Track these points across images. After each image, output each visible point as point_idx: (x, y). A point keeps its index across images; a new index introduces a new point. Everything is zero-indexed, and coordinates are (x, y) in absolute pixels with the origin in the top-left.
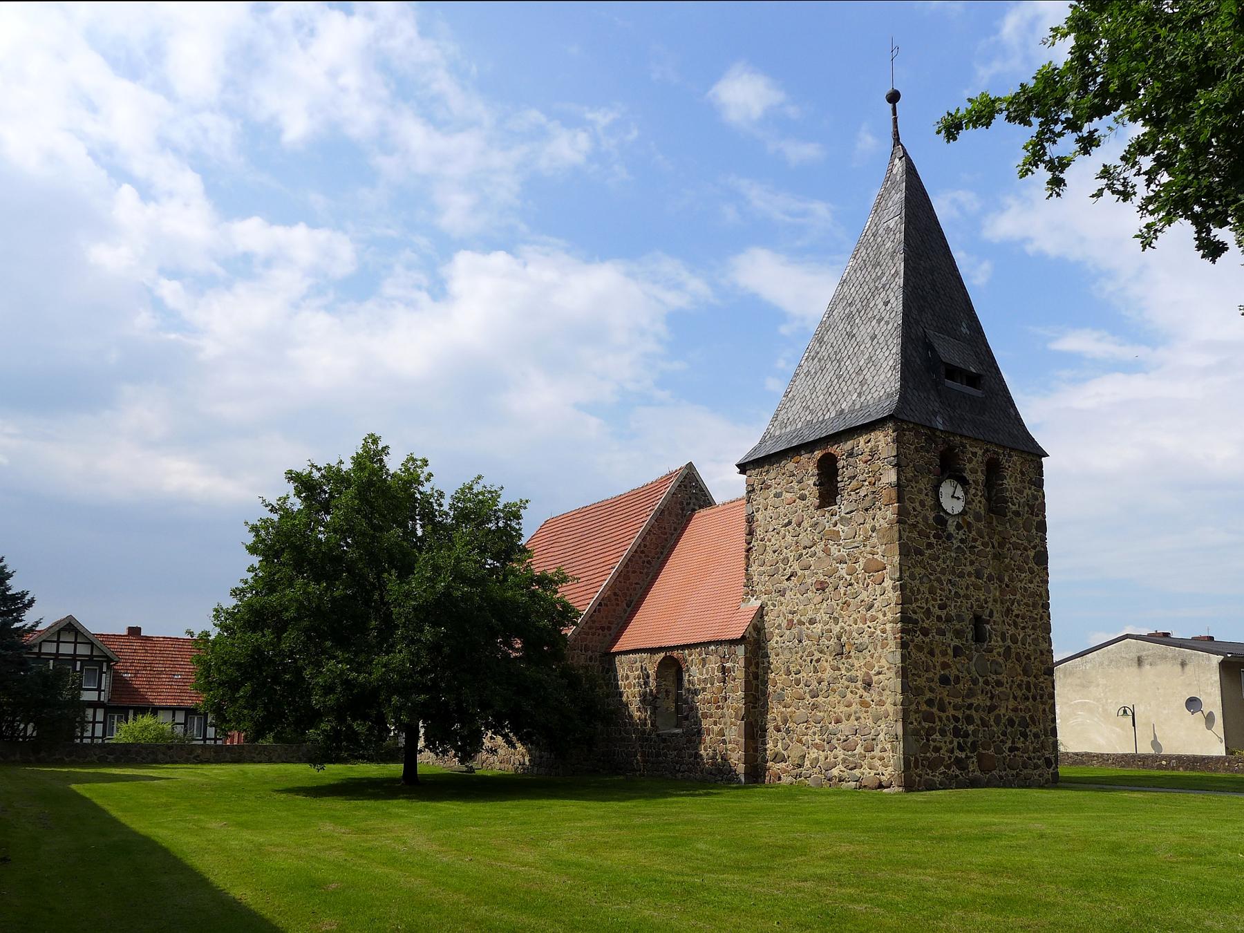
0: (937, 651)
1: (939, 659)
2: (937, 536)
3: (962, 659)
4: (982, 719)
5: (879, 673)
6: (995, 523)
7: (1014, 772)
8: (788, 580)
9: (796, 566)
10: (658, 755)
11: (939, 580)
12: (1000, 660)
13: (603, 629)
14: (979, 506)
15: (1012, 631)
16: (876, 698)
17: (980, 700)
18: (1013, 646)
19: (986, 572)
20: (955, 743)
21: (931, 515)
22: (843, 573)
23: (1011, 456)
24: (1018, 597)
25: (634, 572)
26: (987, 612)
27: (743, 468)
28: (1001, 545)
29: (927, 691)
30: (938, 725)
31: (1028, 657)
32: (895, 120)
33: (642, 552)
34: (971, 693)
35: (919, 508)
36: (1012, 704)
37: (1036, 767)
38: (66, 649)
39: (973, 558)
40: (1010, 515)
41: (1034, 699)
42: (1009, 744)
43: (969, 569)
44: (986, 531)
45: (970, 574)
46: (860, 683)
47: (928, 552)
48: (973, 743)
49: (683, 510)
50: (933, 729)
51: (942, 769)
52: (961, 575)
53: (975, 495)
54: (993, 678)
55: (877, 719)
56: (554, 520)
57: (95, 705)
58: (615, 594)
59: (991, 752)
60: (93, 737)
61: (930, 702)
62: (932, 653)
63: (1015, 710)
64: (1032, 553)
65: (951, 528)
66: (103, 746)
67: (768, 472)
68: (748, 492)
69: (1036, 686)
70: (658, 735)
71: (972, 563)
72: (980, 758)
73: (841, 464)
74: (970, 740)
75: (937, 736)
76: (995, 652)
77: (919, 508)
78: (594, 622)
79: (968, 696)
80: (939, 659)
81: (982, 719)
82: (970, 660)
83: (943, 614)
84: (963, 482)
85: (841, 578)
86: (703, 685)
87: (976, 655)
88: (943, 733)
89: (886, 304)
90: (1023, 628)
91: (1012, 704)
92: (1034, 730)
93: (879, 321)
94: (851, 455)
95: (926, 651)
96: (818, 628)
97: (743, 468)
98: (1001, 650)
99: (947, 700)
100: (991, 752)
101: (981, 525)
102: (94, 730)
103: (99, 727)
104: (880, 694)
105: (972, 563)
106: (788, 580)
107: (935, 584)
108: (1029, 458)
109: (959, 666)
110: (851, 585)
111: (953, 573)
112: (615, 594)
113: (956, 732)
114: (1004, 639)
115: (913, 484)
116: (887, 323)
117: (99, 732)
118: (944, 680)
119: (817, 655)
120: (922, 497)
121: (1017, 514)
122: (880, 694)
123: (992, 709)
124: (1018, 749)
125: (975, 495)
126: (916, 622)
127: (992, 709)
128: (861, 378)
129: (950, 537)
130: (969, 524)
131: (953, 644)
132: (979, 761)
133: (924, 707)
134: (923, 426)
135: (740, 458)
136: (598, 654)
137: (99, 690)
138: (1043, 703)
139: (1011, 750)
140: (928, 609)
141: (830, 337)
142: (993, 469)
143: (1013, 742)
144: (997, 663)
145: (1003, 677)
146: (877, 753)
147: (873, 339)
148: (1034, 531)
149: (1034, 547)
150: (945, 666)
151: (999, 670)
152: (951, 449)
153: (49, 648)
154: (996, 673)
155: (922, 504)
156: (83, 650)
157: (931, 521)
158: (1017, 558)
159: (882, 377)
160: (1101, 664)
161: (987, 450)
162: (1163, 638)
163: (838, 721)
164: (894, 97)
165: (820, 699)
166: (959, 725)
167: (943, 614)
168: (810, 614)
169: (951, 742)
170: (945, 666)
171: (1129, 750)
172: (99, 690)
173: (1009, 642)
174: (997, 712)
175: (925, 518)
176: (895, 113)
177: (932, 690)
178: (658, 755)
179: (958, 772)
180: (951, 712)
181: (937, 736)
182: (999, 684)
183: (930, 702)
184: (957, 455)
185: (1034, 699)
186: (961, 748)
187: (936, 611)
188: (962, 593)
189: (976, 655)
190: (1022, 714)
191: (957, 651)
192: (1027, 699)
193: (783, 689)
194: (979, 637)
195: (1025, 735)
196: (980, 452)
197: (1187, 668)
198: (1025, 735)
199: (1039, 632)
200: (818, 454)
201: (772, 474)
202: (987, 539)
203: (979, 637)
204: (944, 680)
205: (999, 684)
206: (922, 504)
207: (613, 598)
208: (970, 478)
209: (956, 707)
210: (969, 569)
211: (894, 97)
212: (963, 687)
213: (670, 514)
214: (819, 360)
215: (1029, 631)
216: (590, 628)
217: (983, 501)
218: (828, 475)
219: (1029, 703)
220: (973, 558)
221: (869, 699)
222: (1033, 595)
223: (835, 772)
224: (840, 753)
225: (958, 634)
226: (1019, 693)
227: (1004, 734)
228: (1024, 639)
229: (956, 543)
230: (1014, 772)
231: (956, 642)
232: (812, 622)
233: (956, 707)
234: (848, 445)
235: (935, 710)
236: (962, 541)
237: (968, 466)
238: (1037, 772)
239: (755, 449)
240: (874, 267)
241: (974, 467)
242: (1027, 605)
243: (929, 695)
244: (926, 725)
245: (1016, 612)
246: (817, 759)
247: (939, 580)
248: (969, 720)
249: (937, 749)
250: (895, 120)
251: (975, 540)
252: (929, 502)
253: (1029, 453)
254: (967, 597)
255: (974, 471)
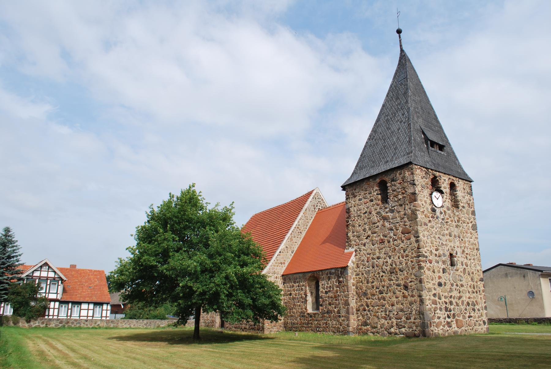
0: (436, 271)
1: (437, 275)
2: (432, 217)
3: (446, 274)
4: (456, 303)
5: (411, 282)
6: (455, 211)
7: (471, 328)
8: (366, 238)
9: (369, 233)
10: (308, 323)
11: (434, 237)
12: (462, 274)
13: (281, 263)
14: (448, 204)
15: (465, 261)
16: (410, 293)
17: (455, 294)
18: (466, 268)
19: (453, 234)
20: (446, 315)
21: (430, 207)
22: (392, 235)
23: (459, 181)
24: (467, 245)
25: (295, 237)
26: (455, 252)
27: (344, 188)
28: (458, 221)
29: (433, 289)
30: (438, 306)
31: (473, 273)
32: (400, 41)
33: (298, 228)
34: (451, 290)
35: (424, 204)
36: (468, 295)
37: (480, 325)
38: (44, 274)
39: (448, 227)
40: (461, 208)
41: (477, 292)
42: (468, 315)
43: (446, 232)
44: (452, 215)
45: (447, 234)
46: (402, 287)
47: (429, 224)
48: (454, 314)
49: (315, 209)
50: (436, 308)
51: (441, 327)
52: (443, 235)
53: (446, 199)
54: (459, 283)
55: (411, 303)
56: (256, 215)
57: (55, 300)
58: (287, 247)
59: (461, 318)
60: (53, 316)
61: (434, 295)
62: (434, 272)
63: (469, 298)
64: (470, 225)
65: (438, 213)
66: (58, 320)
67: (355, 190)
68: (347, 199)
69: (477, 286)
70: (308, 314)
71: (447, 229)
72: (457, 321)
73: (389, 185)
74: (452, 312)
75: (438, 311)
76: (459, 271)
77: (424, 204)
78: (277, 260)
79: (450, 292)
80: (437, 275)
81: (456, 303)
82: (450, 274)
83: (437, 253)
84: (441, 192)
85: (391, 237)
86: (329, 289)
87: (452, 272)
88: (441, 309)
89: (403, 115)
90: (470, 259)
91: (468, 295)
92: (478, 307)
93: (401, 122)
94: (393, 180)
95: (431, 270)
96: (381, 261)
97: (344, 188)
98: (462, 270)
99: (441, 294)
100: (461, 318)
101: (449, 212)
102: (55, 311)
103: (56, 311)
104: (412, 291)
105: (447, 229)
106: (366, 238)
107: (433, 239)
108: (466, 182)
109: (445, 277)
110: (396, 240)
111: (440, 234)
112: (287, 247)
113: (446, 309)
114: (462, 265)
115: (421, 193)
116: (404, 123)
117: (56, 314)
118: (440, 284)
119: (382, 274)
120: (425, 199)
121: (463, 207)
122: (412, 291)
123: (460, 298)
124: (471, 317)
125: (446, 199)
126: (427, 257)
127: (460, 298)
128: (395, 147)
129: (437, 218)
130: (445, 212)
131: (442, 267)
132: (457, 323)
133: (432, 298)
134: (424, 167)
135: (342, 183)
136: (279, 275)
137: (57, 293)
138: (480, 294)
139: (469, 317)
140: (431, 251)
141: (380, 130)
142: (452, 186)
143: (470, 313)
144: (461, 276)
145: (464, 283)
146: (412, 320)
147: (398, 130)
148: (470, 215)
149: (471, 222)
150: (440, 277)
151: (462, 279)
152: (435, 177)
153: (37, 274)
154: (461, 281)
155: (426, 203)
156: (51, 275)
157: (430, 210)
158: (465, 227)
159: (404, 145)
160: (490, 277)
161: (450, 179)
162: (511, 266)
163: (393, 305)
164: (399, 32)
165: (384, 295)
166: (447, 306)
167: (437, 253)
168: (378, 254)
169: (444, 314)
170: (440, 277)
171: (505, 317)
172: (57, 293)
173: (464, 266)
174: (462, 299)
175: (427, 209)
176: (400, 38)
177: (435, 289)
178: (308, 323)
179: (448, 329)
180: (443, 299)
181: (438, 311)
182: (462, 286)
183: (434, 295)
184: (438, 180)
185: (477, 292)
186: (449, 317)
187: (434, 252)
188: (444, 243)
189: (452, 272)
190: (472, 300)
191: (444, 271)
192: (474, 292)
193: (366, 291)
194: (452, 264)
195: (474, 310)
196: (447, 180)
197: (526, 278)
198: (474, 310)
199: (476, 261)
200: (378, 180)
201: (357, 191)
202: (452, 219)
203: (452, 264)
204: (440, 284)
205: (462, 286)
206: (426, 203)
207: (286, 249)
208: (444, 191)
209: (445, 297)
210: (446, 232)
211: (399, 32)
212: (448, 287)
213: (309, 210)
214: (375, 140)
215: (472, 261)
216: (276, 263)
217: (450, 201)
218: (383, 188)
219: (475, 295)
220: (448, 227)
221: (407, 294)
222: (472, 244)
223: (392, 330)
224: (394, 321)
225: (444, 262)
226: (470, 290)
227: (466, 310)
228: (471, 264)
229: (441, 221)
230: (471, 328)
231: (443, 266)
232: (378, 258)
233: (445, 297)
234: (392, 176)
235: (437, 299)
236: (443, 219)
237: (443, 186)
238: (480, 327)
239: (349, 180)
240: (396, 99)
241: (445, 185)
242: (470, 249)
243: (434, 292)
244: (434, 306)
245: (466, 252)
246: (383, 324)
247: (434, 237)
248: (451, 303)
249: (439, 318)
250: (400, 41)
251: (448, 219)
252: (429, 201)
253: (466, 180)
254: (446, 245)
255: (445, 188)
